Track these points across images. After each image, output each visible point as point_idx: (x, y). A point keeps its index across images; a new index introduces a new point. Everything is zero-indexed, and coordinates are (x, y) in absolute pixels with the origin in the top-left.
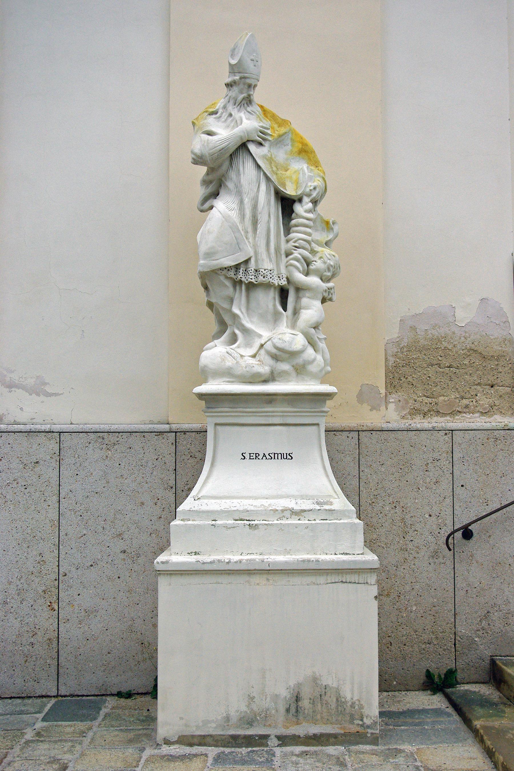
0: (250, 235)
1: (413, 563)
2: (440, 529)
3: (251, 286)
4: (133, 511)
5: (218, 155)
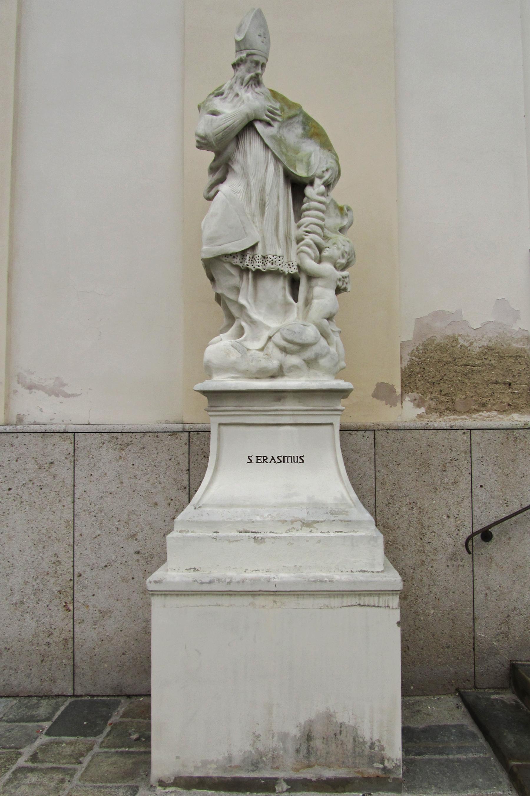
0: (257, 219)
1: (430, 565)
2: (459, 530)
3: (258, 274)
4: (146, 511)
5: (222, 135)
